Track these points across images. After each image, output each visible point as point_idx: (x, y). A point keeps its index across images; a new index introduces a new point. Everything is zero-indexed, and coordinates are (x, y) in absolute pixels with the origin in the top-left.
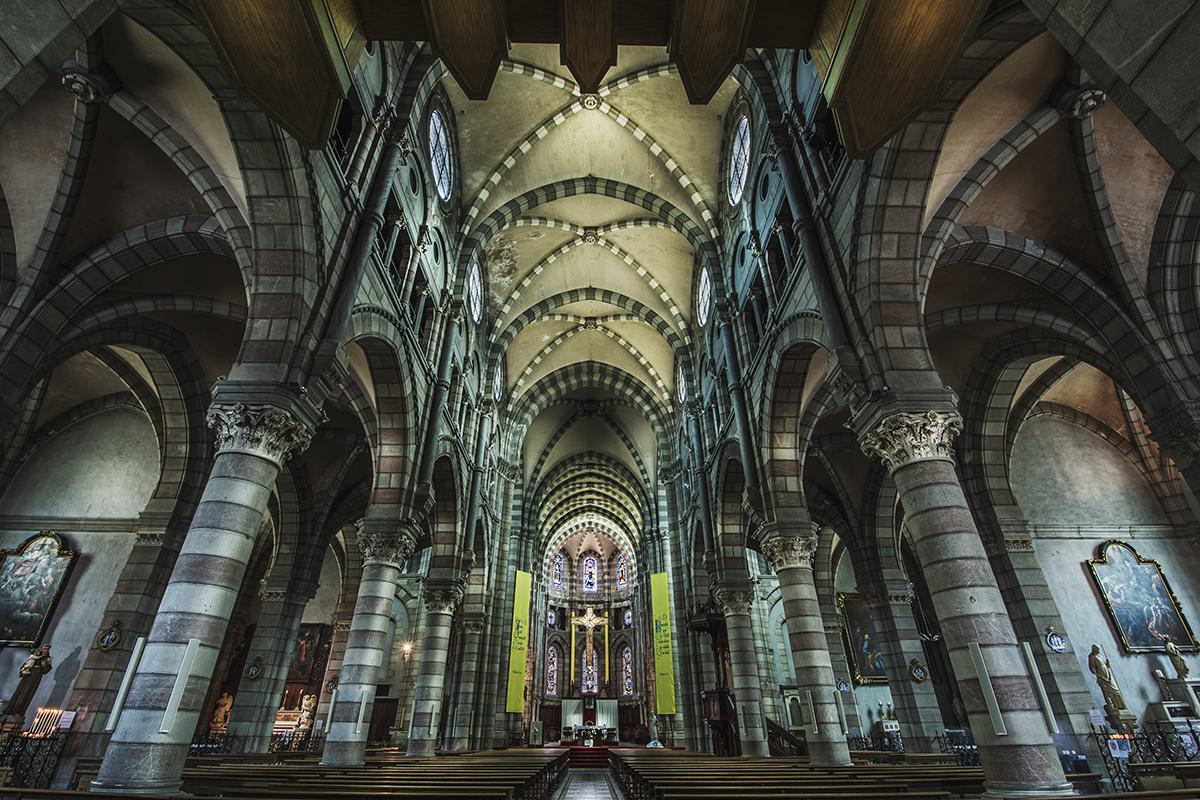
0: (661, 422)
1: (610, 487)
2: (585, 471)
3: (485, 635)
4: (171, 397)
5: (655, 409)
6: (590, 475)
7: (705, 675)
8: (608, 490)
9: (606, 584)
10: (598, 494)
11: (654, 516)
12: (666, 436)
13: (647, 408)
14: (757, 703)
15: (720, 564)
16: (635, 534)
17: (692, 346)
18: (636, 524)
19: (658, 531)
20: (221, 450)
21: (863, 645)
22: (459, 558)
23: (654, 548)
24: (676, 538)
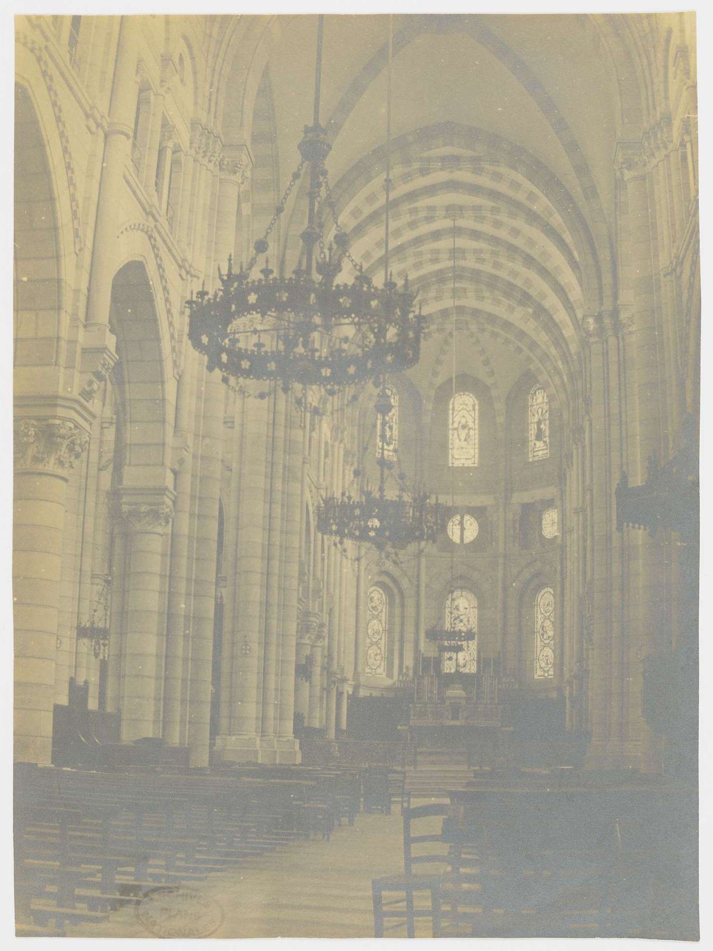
1: (503, 169)
2: (442, 176)
3: (174, 536)
6: (453, 186)
8: (498, 224)
9: (376, 751)
10: (476, 235)
14: (320, 649)
16: (569, 332)
18: (569, 306)
19: (615, 313)
22: (73, 342)
23: (605, 354)
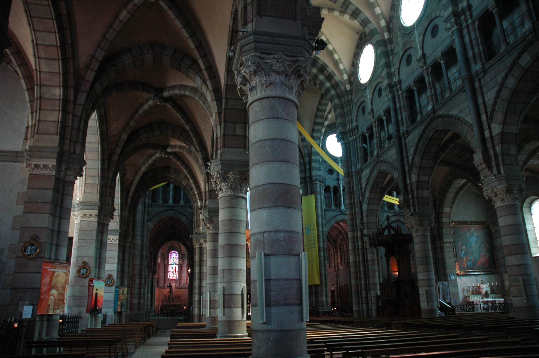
0: (339, 97)
4: (47, 43)
5: (336, 86)
7: (370, 273)
11: (308, 167)
12: (343, 108)
13: (328, 84)
15: (413, 202)
17: (390, 40)
20: (250, 101)
21: (461, 253)
24: (350, 183)
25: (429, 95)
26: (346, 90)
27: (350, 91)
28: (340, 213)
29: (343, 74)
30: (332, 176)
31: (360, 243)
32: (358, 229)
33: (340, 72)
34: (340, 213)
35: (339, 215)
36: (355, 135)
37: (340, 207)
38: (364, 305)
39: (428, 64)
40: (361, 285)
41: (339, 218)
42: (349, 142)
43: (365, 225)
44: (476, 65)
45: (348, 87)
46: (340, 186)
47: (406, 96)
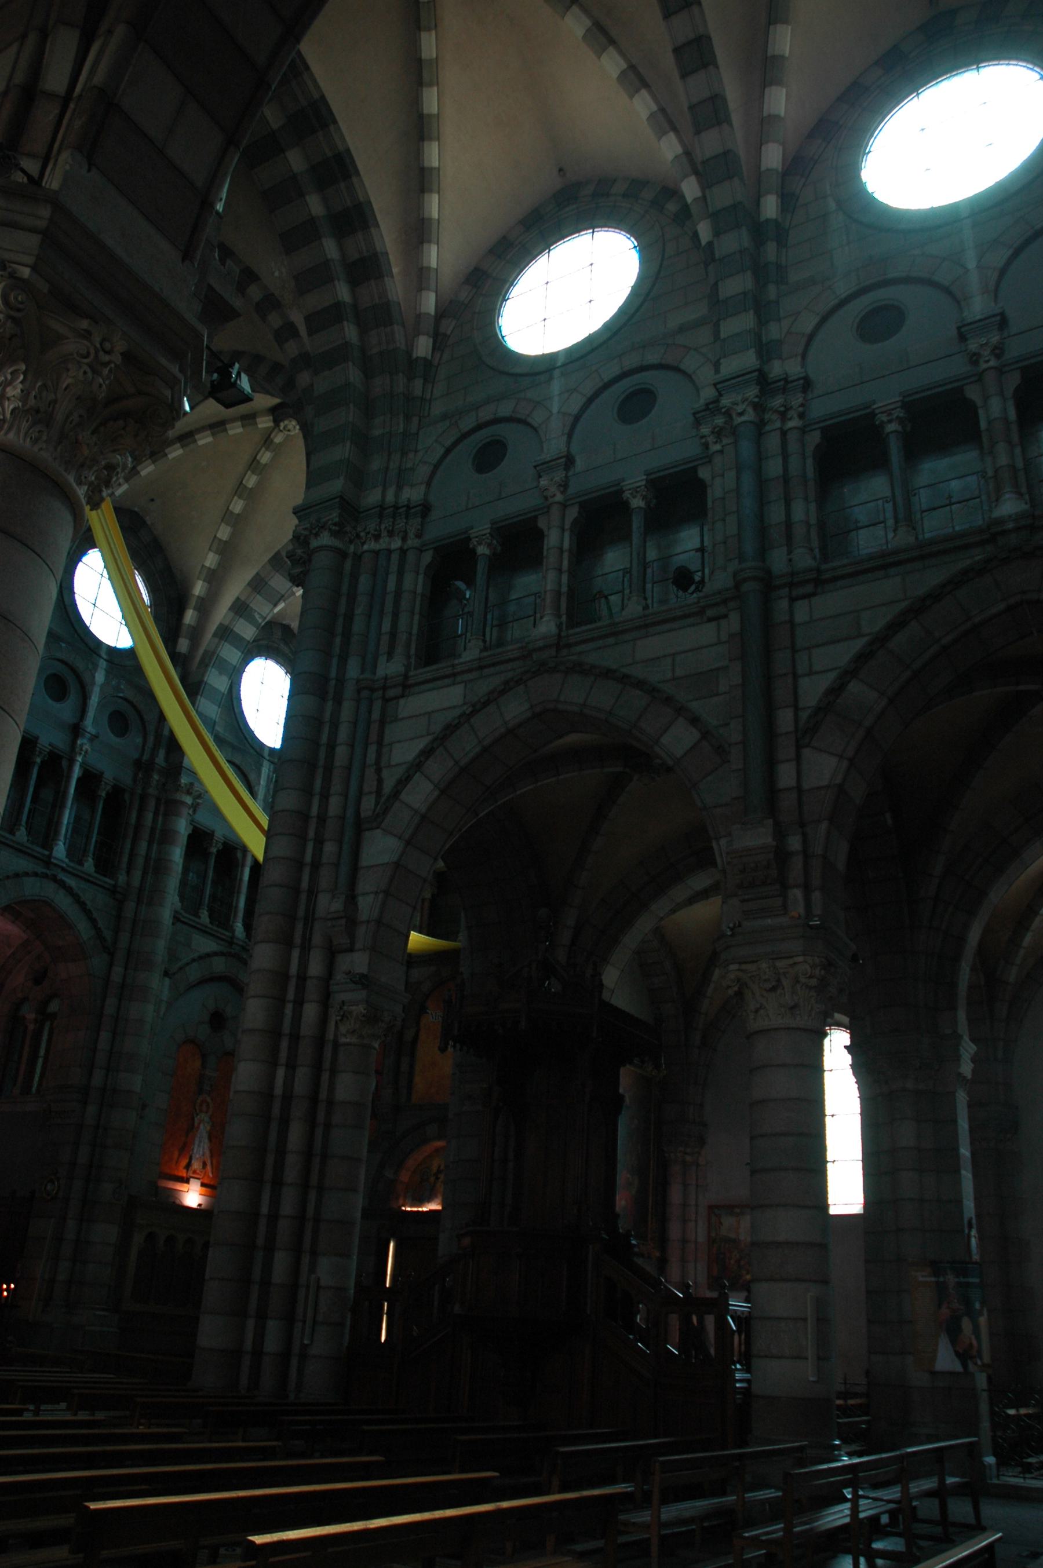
25: (549, 588)
26: (409, 353)
27: (427, 363)
28: (40, 869)
29: (420, 289)
30: (57, 705)
31: (311, 1011)
32: (317, 939)
33: (420, 276)
34: (40, 869)
35: (36, 874)
36: (404, 539)
37: (48, 841)
38: (273, 1328)
39: (571, 491)
40: (274, 1217)
41: (32, 888)
42: (358, 557)
43: (361, 931)
44: (388, 661)
45: (423, 347)
46: (72, 761)
47: (575, 522)
